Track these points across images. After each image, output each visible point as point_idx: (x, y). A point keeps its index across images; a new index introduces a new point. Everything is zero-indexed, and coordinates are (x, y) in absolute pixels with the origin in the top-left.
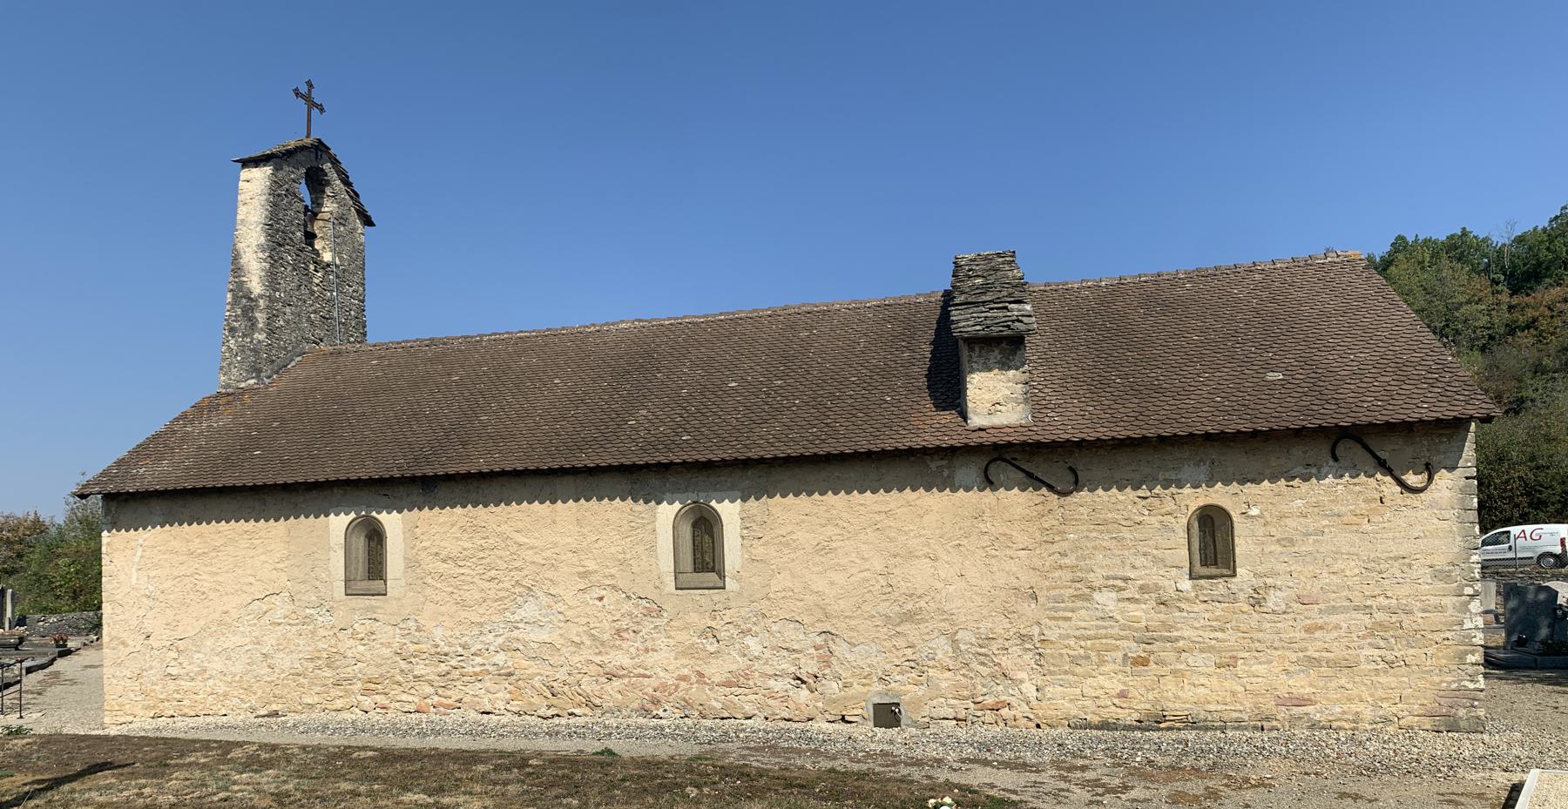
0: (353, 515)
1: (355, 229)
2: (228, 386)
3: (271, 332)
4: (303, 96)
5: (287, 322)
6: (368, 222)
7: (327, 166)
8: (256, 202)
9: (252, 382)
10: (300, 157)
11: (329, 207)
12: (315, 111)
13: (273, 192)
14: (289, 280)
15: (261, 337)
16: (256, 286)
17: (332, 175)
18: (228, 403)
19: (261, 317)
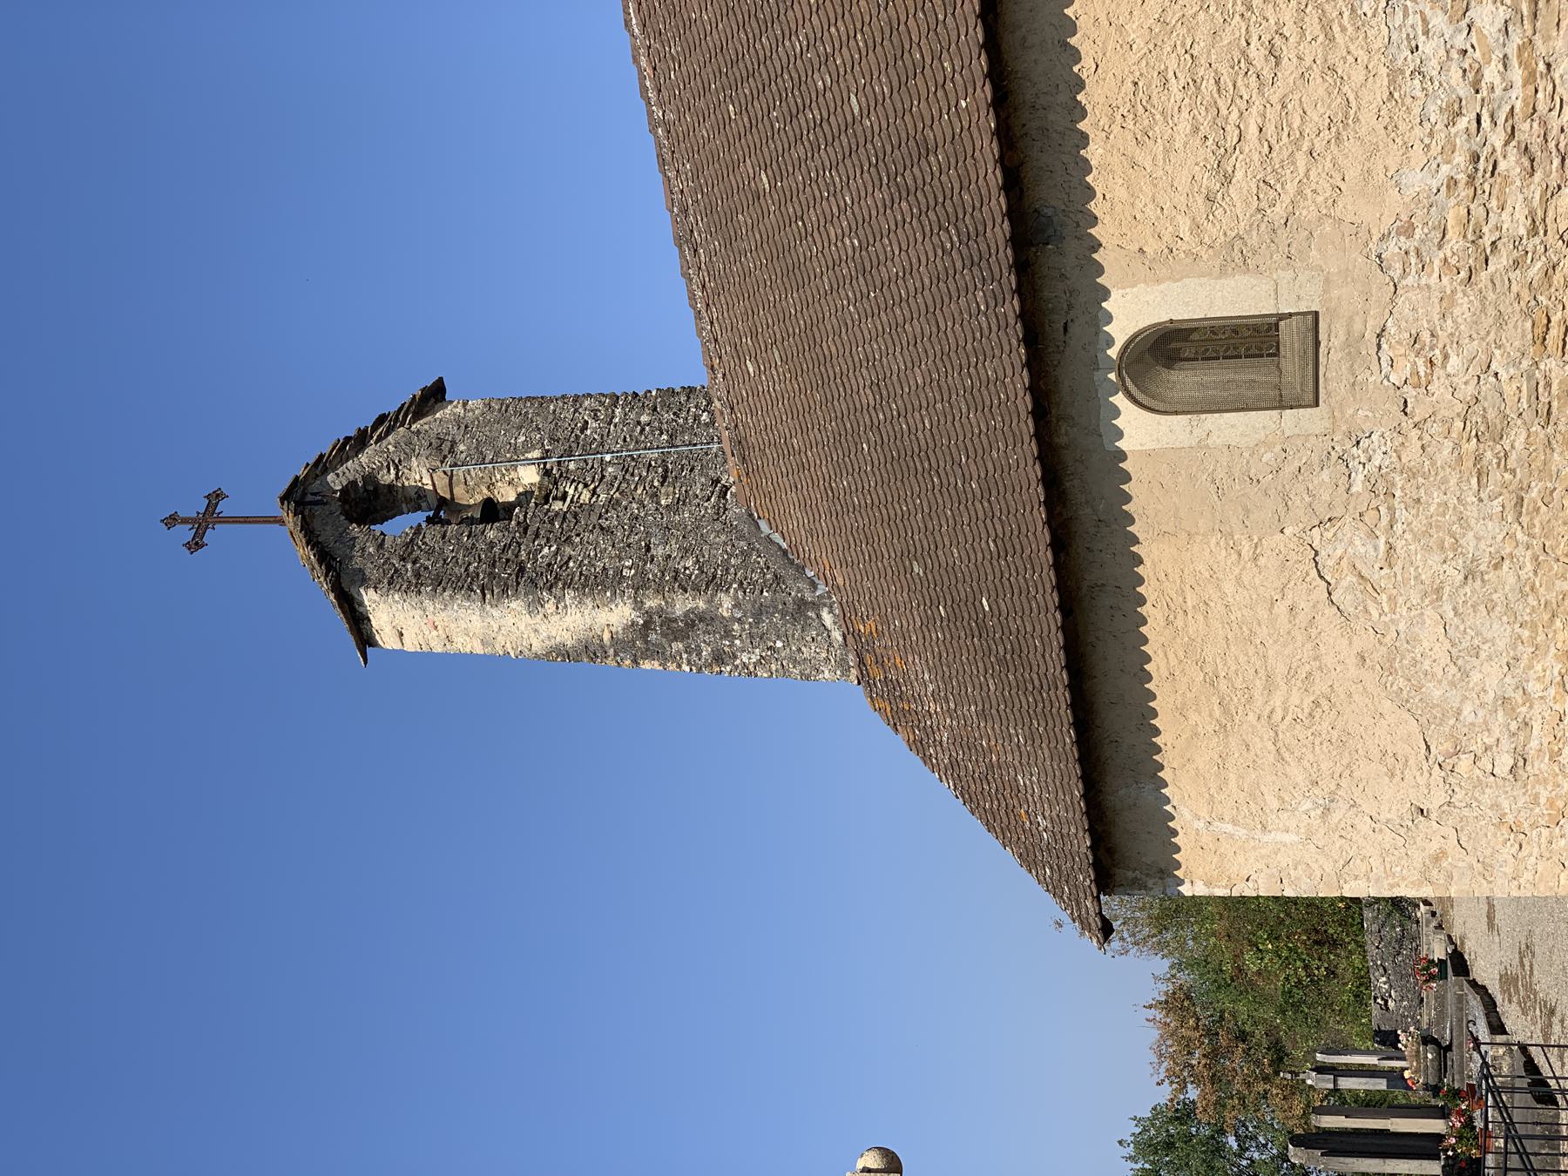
0: (1119, 400)
1: (458, 421)
3: (712, 583)
5: (686, 552)
6: (435, 395)
7: (335, 481)
9: (827, 619)
10: (327, 535)
11: (419, 474)
12: (224, 508)
15: (725, 604)
16: (617, 615)
19: (682, 604)
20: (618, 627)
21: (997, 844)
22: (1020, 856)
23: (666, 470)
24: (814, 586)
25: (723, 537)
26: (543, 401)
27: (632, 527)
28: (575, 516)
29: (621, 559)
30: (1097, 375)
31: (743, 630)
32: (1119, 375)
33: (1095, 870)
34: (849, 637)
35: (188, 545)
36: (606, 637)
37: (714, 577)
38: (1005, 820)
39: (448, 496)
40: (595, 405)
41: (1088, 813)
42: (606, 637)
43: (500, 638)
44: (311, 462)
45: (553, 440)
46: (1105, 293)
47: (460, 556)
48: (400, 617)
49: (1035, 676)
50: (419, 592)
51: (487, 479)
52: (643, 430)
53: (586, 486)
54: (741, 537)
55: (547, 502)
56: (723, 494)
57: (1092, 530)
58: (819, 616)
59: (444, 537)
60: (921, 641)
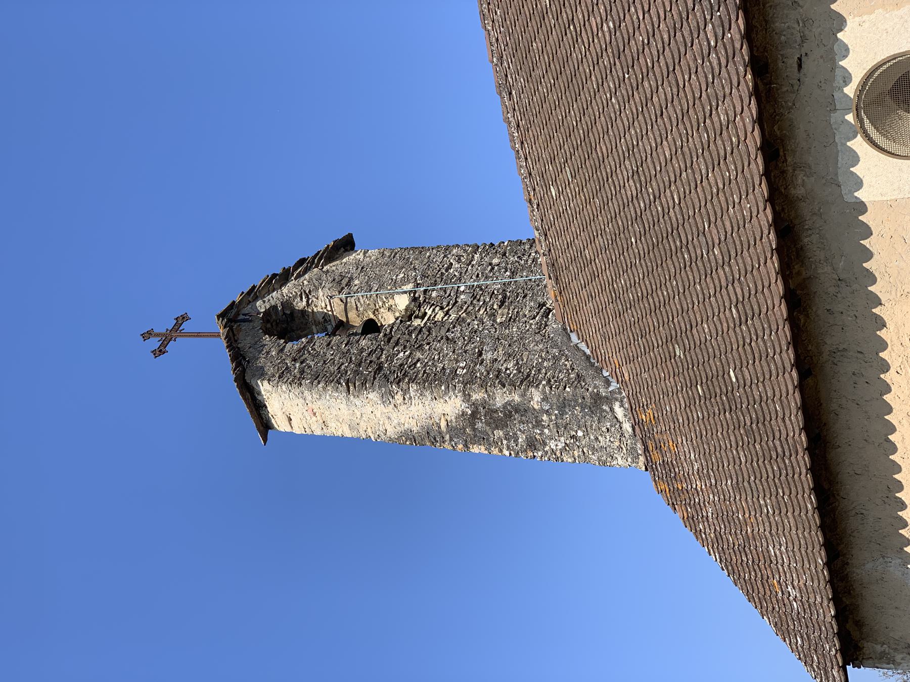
0: (858, 144)
1: (357, 264)
2: (632, 451)
3: (527, 380)
4: (164, 344)
5: (509, 356)
6: (346, 245)
7: (261, 306)
8: (318, 405)
9: (619, 412)
10: (245, 342)
11: (324, 302)
12: (186, 327)
13: (298, 381)
14: (444, 356)
15: (536, 397)
16: (449, 407)
17: (275, 298)
18: (658, 448)
19: (501, 398)
20: (452, 417)
21: (757, 612)
22: (776, 625)
23: (505, 297)
24: (608, 383)
25: (541, 346)
26: (422, 250)
27: (470, 338)
28: (429, 330)
29: (457, 361)
30: (834, 117)
31: (551, 420)
32: (858, 116)
33: (840, 640)
34: (637, 427)
35: (154, 352)
36: (443, 424)
37: (528, 376)
38: (761, 590)
39: (344, 320)
40: (461, 252)
41: (831, 582)
42: (443, 424)
43: (362, 424)
44: (245, 292)
45: (423, 276)
46: (840, 22)
47: (337, 358)
48: (288, 403)
49: (777, 443)
50: (301, 384)
51: (372, 306)
52: (493, 268)
53: (442, 308)
54: (555, 345)
55: (410, 319)
56: (546, 314)
57: (832, 290)
58: (612, 410)
59: (328, 345)
60: (686, 422)
